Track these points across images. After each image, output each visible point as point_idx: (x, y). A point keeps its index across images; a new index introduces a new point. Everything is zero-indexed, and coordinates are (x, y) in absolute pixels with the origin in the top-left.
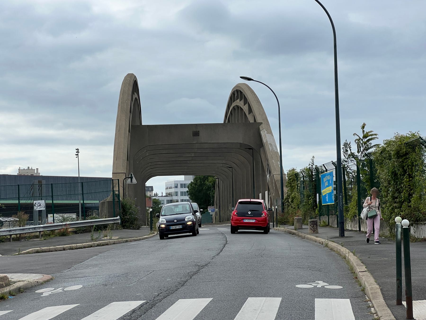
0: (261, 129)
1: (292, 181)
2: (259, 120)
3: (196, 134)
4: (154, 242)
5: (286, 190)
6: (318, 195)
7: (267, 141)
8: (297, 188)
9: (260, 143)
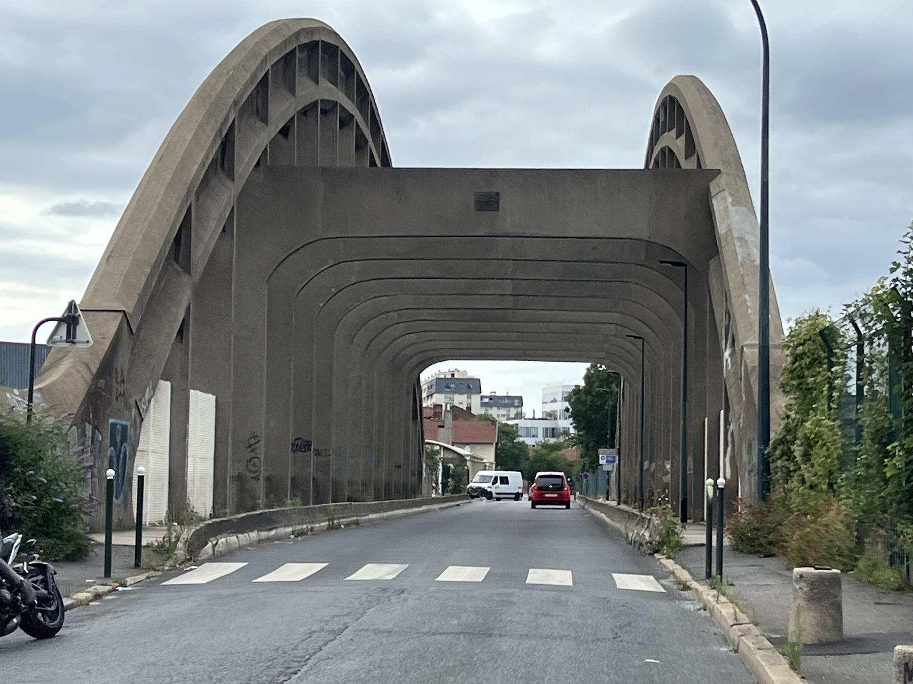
0: (713, 191)
1: (810, 366)
2: (710, 161)
3: (488, 203)
4: (638, 486)
5: (780, 402)
6: (722, 412)
7: (730, 230)
8: (830, 397)
9: (709, 242)
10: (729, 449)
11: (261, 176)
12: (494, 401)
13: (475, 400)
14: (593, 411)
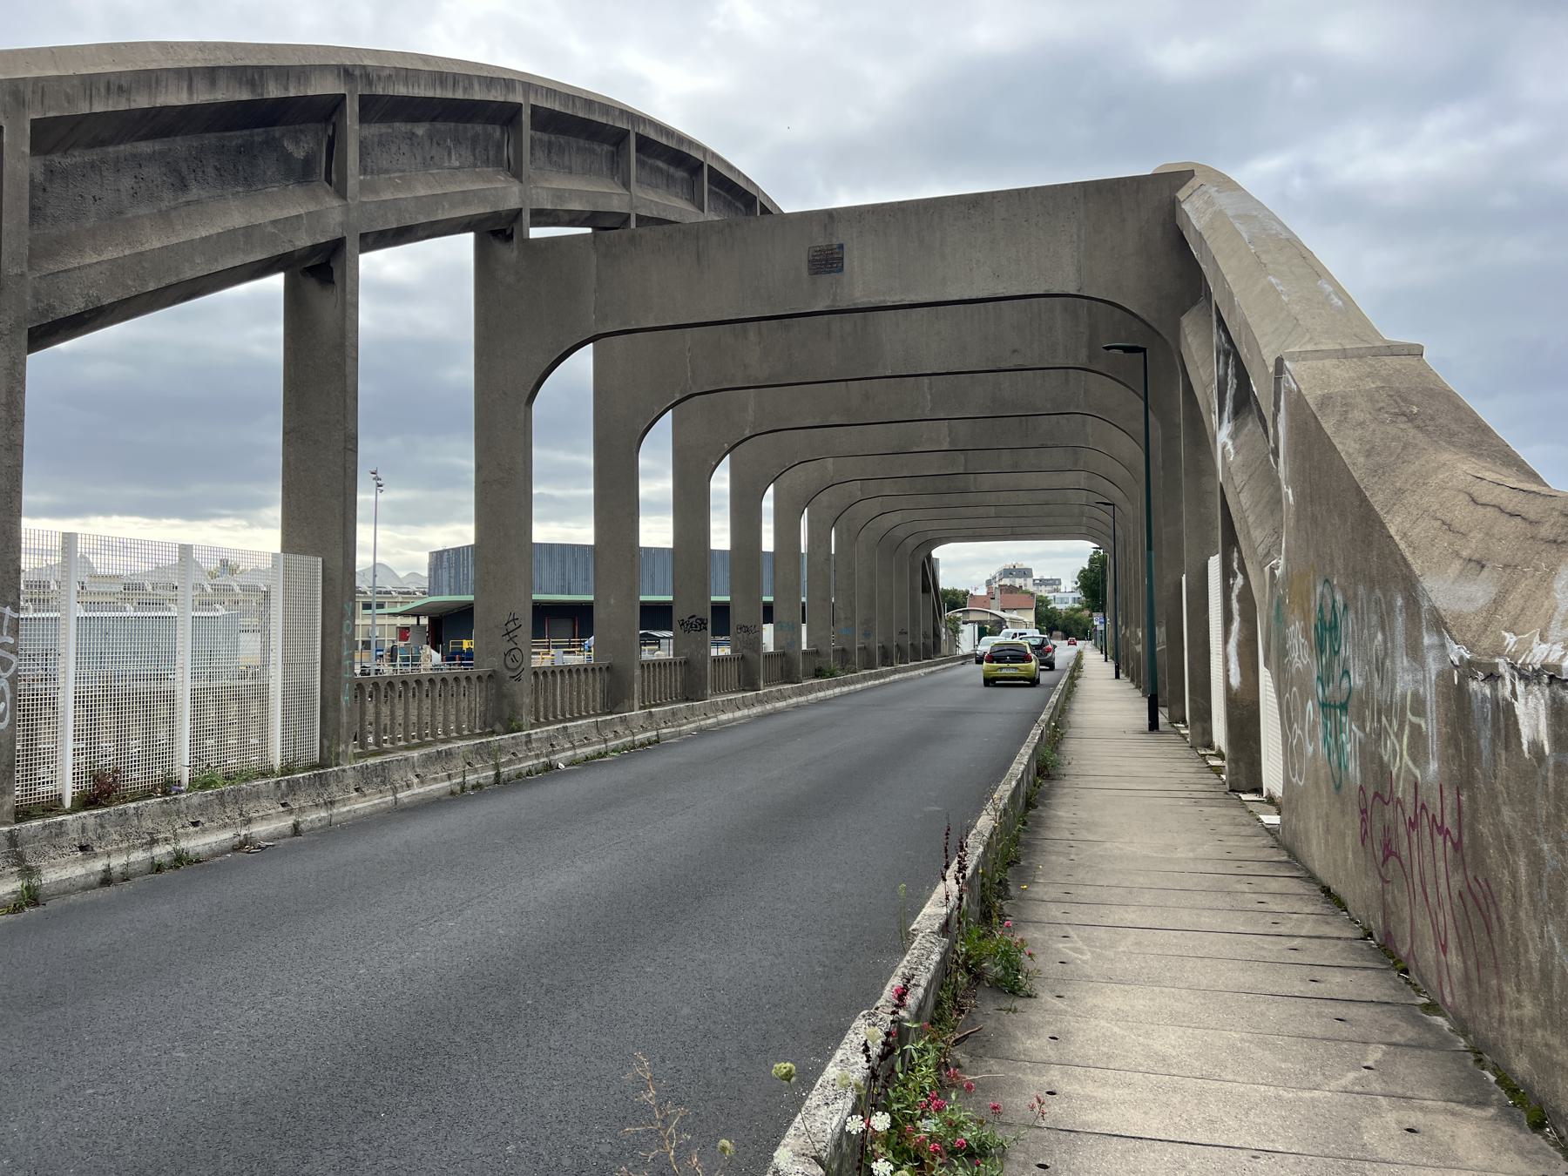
3: (828, 261)
10: (1235, 626)
11: (515, 253)
12: (1043, 582)
13: (1030, 581)
14: (1092, 584)
